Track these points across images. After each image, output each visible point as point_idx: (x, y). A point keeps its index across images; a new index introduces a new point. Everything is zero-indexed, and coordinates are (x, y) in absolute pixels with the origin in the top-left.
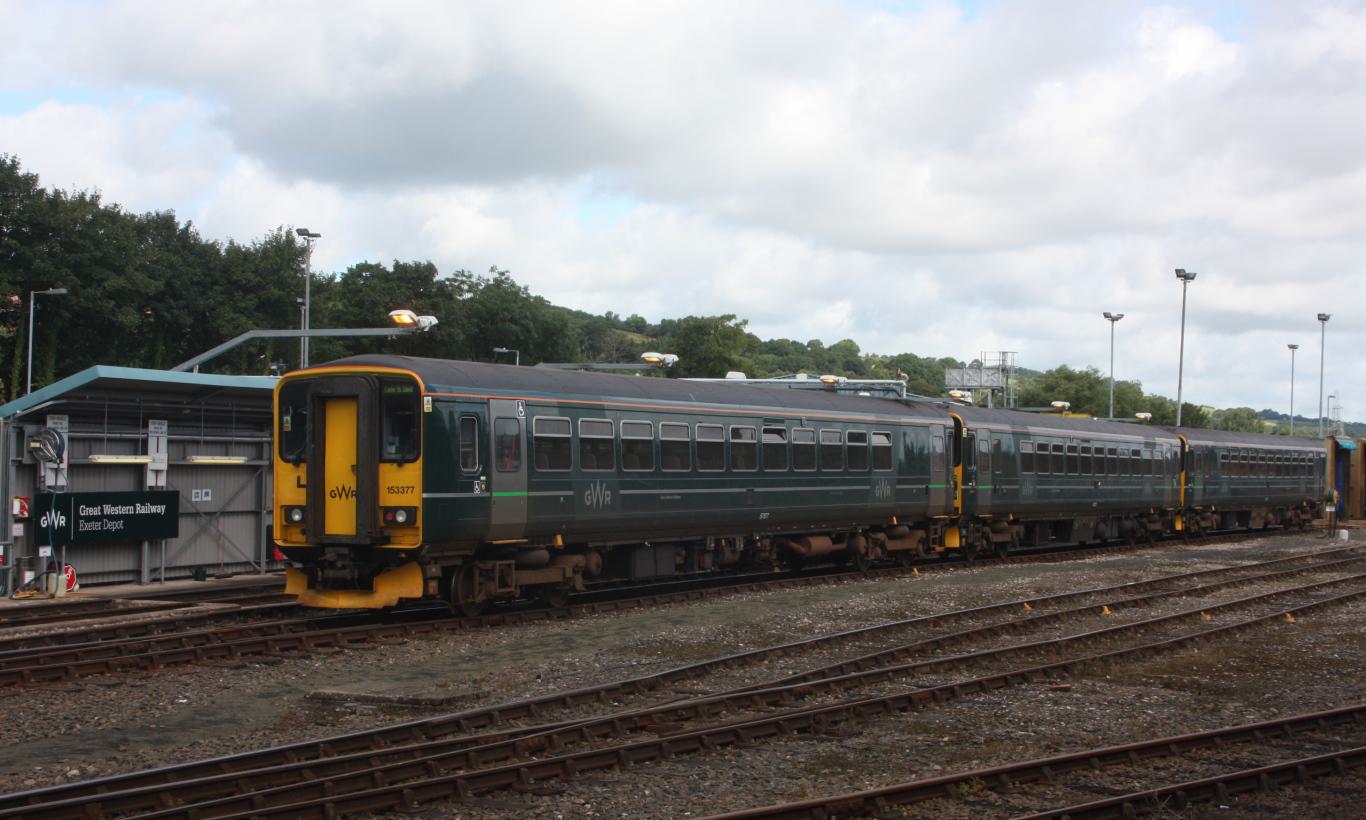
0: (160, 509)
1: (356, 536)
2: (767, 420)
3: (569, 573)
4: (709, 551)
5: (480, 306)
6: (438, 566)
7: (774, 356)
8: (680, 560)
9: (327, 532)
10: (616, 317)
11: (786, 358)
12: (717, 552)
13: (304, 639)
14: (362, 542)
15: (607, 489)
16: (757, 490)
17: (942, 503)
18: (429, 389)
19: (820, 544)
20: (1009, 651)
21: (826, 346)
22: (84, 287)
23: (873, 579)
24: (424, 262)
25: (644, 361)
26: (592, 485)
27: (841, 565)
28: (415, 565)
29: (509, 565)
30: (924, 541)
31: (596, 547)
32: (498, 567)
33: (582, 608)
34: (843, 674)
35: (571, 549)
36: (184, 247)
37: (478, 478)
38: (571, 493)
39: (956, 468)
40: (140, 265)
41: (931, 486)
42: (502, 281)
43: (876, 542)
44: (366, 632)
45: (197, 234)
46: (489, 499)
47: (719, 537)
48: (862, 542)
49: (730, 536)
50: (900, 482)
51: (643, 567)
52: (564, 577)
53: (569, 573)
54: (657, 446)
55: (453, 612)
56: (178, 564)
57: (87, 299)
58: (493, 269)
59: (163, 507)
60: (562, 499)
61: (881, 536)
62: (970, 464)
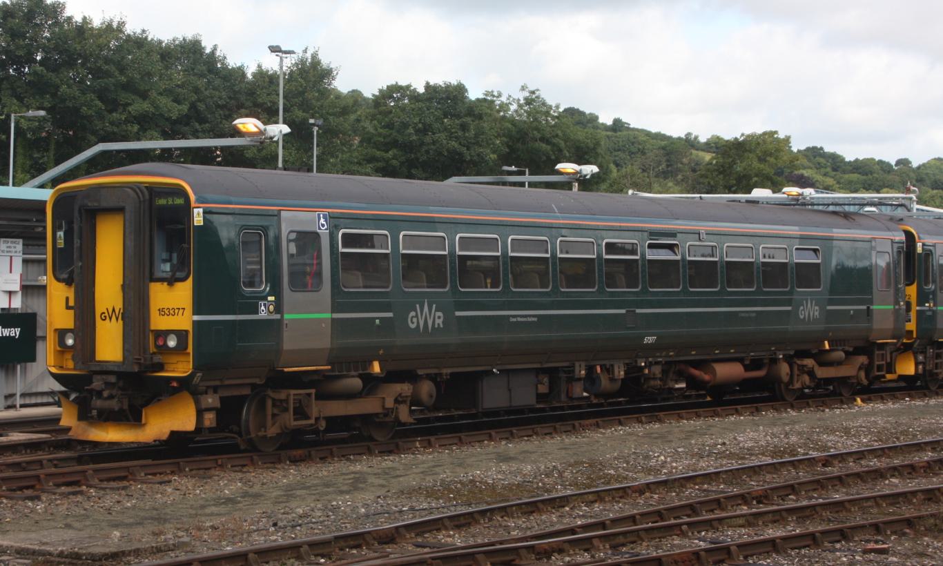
0: (15, 332)
1: (123, 362)
2: (653, 234)
3: (390, 403)
4: (579, 379)
5: (510, 126)
6: (217, 397)
7: (859, 175)
8: (543, 389)
9: (97, 359)
10: (696, 138)
11: (870, 177)
12: (591, 378)
13: (42, 476)
14: (129, 369)
15: (437, 310)
16: (638, 311)
17: (889, 324)
18: (201, 200)
19: (728, 371)
20: (868, 499)
21: (915, 164)
22: (110, 112)
23: (799, 409)
24: (454, 82)
25: (559, 173)
26: (805, 302)
27: (760, 393)
28: (186, 394)
29: (309, 395)
30: (868, 369)
31: (427, 375)
32: (292, 397)
33: (415, 441)
34: (636, 525)
36: (210, 71)
37: (265, 298)
38: (390, 315)
39: (908, 288)
40: (165, 90)
41: (872, 307)
42: (533, 100)
43: (802, 369)
44: (128, 468)
45: (225, 58)
46: (279, 322)
47: (593, 363)
48: (784, 369)
49: (607, 363)
50: (831, 302)
51: (493, 396)
52: (383, 407)
53: (390, 403)
54: (792, 268)
55: (242, 447)
56: (40, 389)
57: (112, 123)
58: (523, 88)
59: (18, 331)
60: (852, 312)
61: (809, 362)
62: (927, 283)
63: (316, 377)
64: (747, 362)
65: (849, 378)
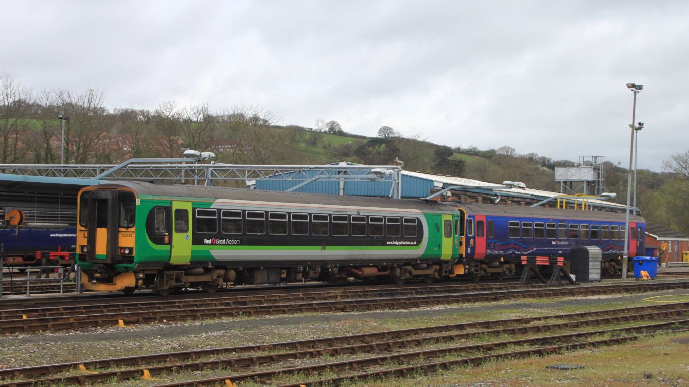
3: (505, 269)
29: (182, 273)
35: (505, 262)
43: (406, 271)
48: (399, 270)
53: (505, 269)
63: (185, 267)
64: (380, 267)
65: (429, 275)
